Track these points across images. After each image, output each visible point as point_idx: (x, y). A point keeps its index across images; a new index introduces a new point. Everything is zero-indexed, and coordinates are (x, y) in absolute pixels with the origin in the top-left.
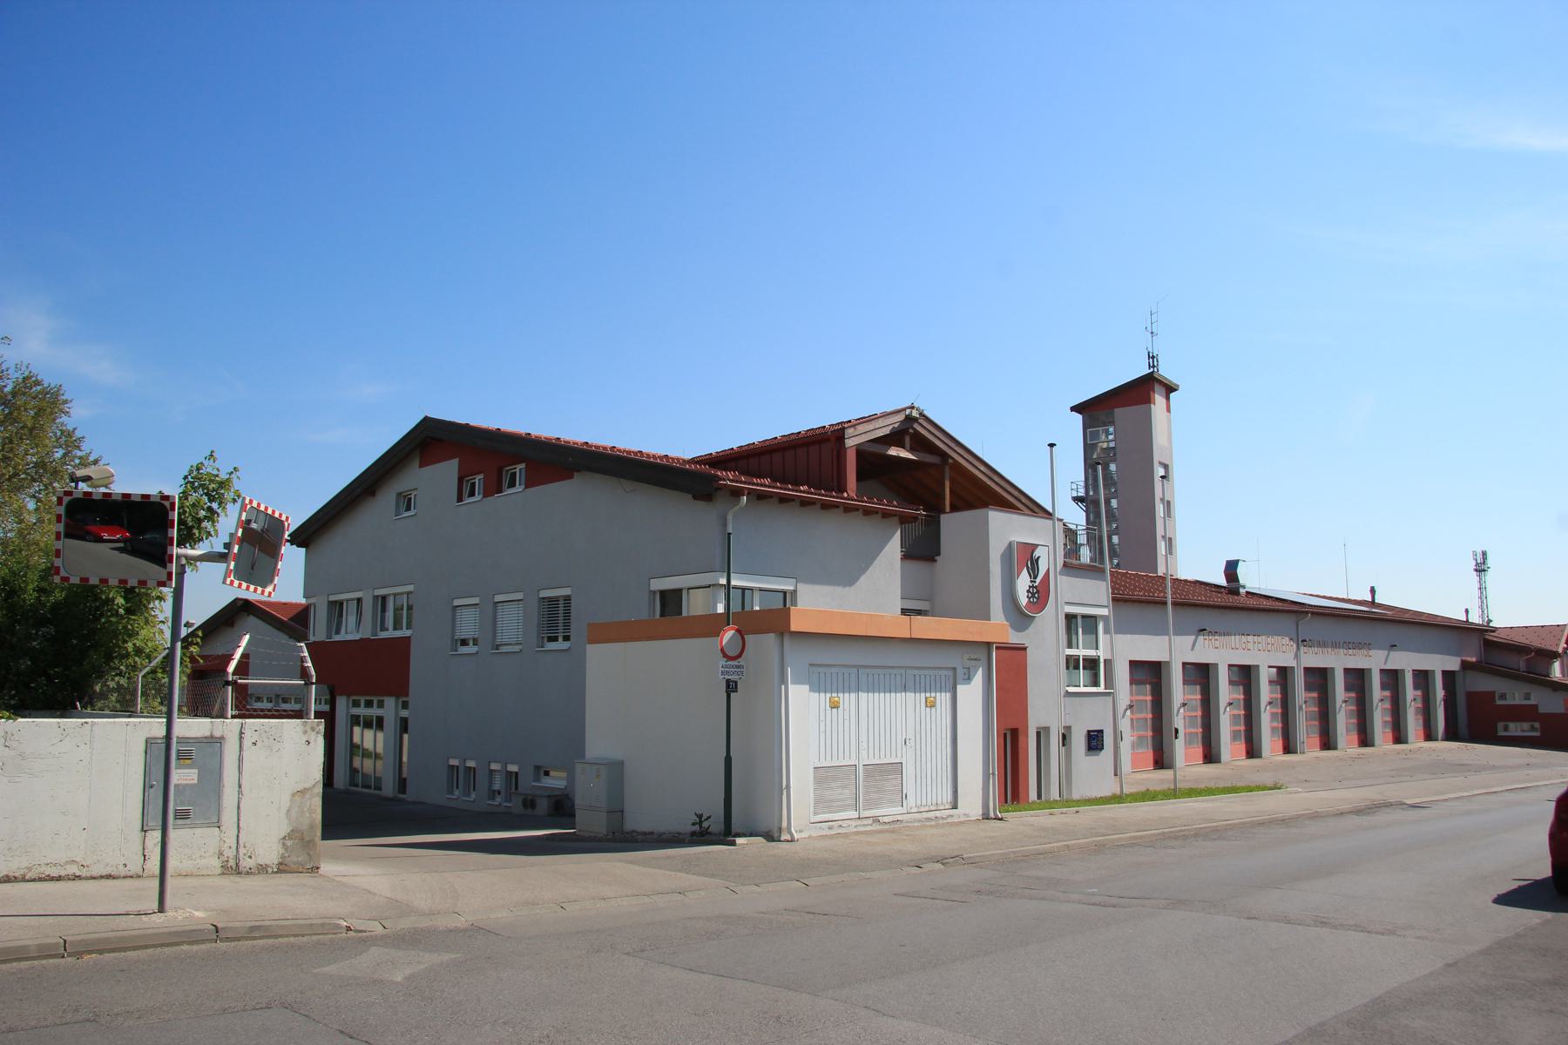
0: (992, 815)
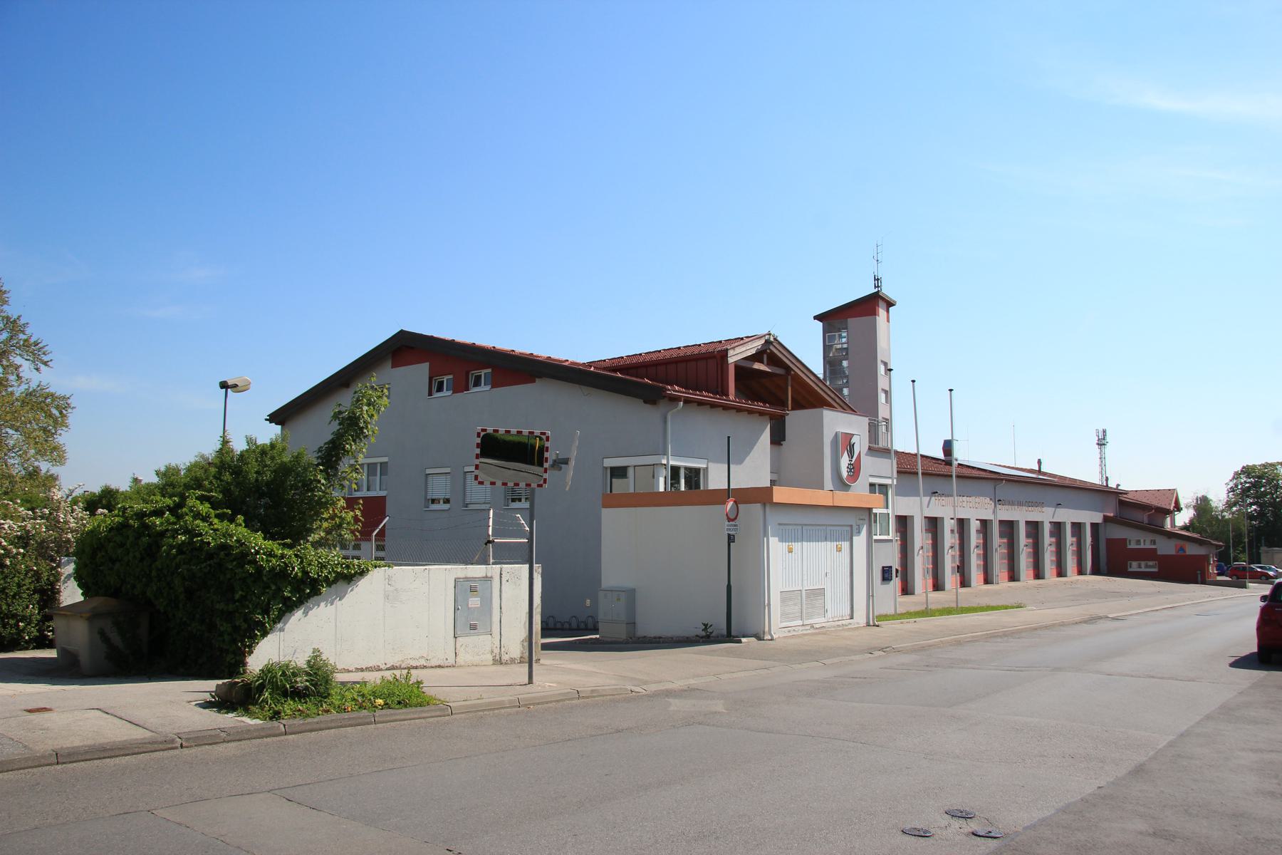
0: (871, 623)
